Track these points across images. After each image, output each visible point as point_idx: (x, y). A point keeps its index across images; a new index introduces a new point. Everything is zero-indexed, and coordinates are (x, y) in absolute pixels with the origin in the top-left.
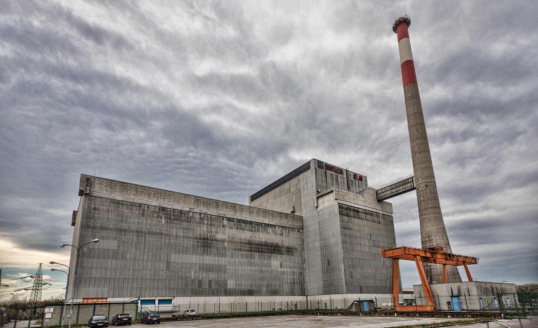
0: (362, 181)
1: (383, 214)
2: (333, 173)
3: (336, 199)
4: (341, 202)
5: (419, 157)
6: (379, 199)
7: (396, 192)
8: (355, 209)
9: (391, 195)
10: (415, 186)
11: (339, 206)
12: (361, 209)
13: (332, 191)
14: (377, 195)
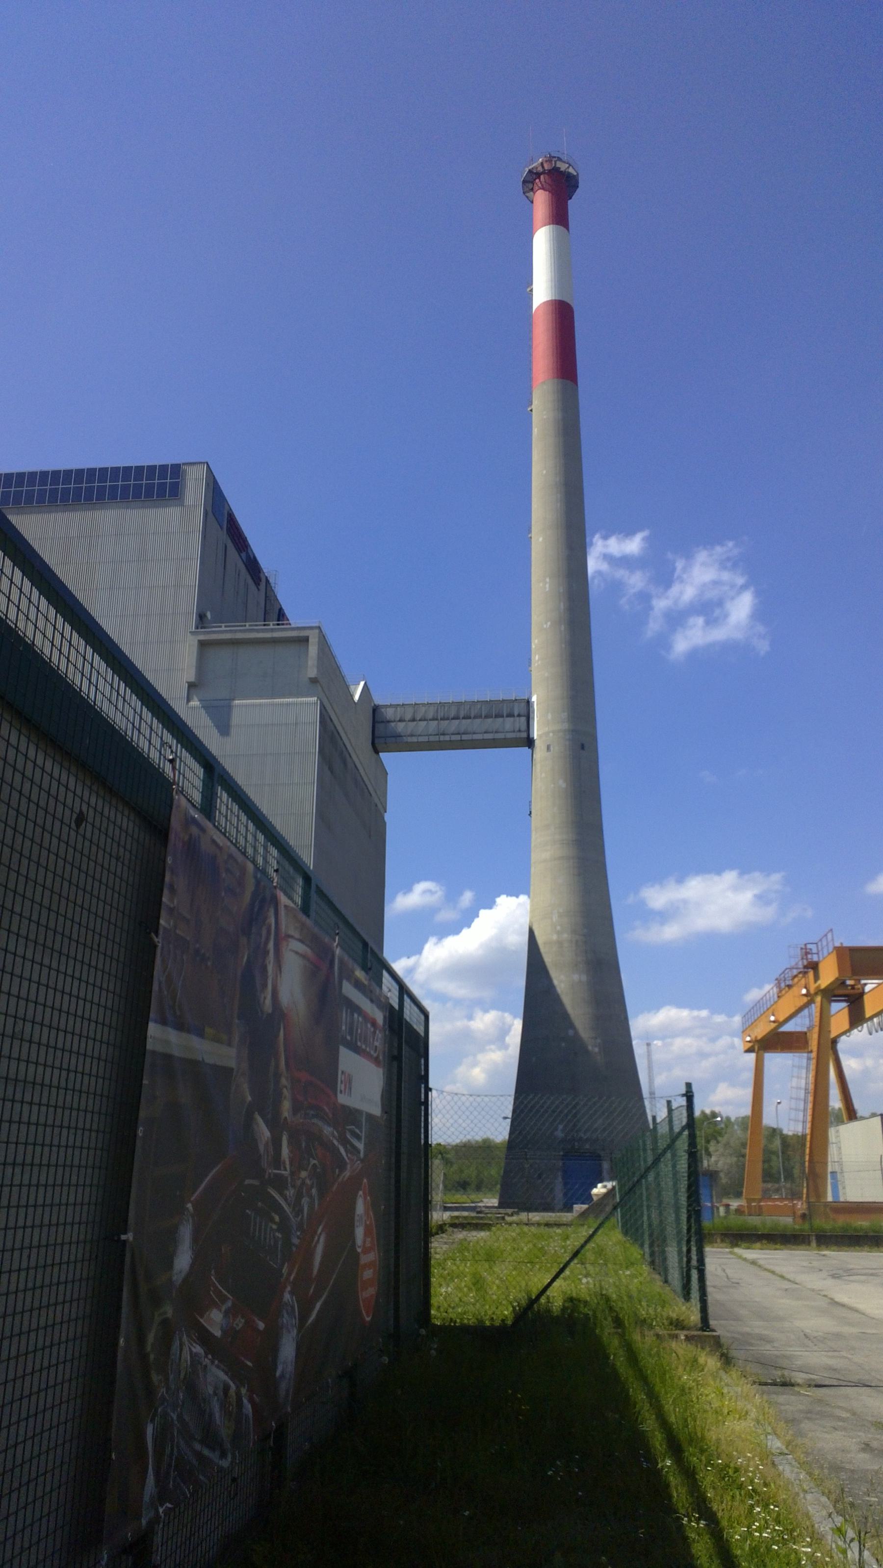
9: (436, 738)
14: (377, 725)
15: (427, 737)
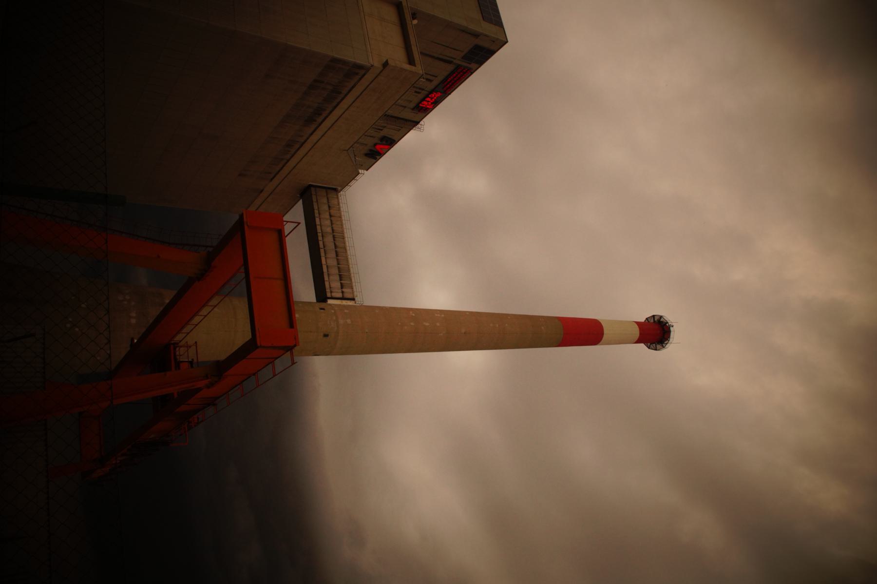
0: (366, 155)
1: (262, 191)
2: (436, 82)
3: (386, 64)
4: (369, 77)
5: (406, 327)
6: (313, 193)
7: (324, 247)
8: (320, 114)
10: (330, 301)
11: (360, 67)
12: (312, 134)
13: (411, 61)
15: (319, 224)
